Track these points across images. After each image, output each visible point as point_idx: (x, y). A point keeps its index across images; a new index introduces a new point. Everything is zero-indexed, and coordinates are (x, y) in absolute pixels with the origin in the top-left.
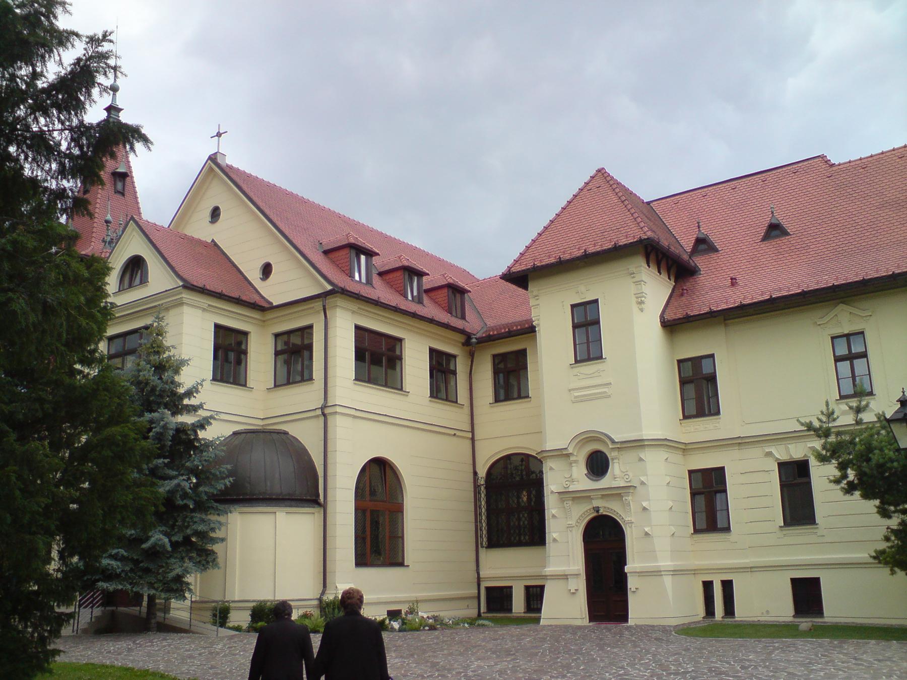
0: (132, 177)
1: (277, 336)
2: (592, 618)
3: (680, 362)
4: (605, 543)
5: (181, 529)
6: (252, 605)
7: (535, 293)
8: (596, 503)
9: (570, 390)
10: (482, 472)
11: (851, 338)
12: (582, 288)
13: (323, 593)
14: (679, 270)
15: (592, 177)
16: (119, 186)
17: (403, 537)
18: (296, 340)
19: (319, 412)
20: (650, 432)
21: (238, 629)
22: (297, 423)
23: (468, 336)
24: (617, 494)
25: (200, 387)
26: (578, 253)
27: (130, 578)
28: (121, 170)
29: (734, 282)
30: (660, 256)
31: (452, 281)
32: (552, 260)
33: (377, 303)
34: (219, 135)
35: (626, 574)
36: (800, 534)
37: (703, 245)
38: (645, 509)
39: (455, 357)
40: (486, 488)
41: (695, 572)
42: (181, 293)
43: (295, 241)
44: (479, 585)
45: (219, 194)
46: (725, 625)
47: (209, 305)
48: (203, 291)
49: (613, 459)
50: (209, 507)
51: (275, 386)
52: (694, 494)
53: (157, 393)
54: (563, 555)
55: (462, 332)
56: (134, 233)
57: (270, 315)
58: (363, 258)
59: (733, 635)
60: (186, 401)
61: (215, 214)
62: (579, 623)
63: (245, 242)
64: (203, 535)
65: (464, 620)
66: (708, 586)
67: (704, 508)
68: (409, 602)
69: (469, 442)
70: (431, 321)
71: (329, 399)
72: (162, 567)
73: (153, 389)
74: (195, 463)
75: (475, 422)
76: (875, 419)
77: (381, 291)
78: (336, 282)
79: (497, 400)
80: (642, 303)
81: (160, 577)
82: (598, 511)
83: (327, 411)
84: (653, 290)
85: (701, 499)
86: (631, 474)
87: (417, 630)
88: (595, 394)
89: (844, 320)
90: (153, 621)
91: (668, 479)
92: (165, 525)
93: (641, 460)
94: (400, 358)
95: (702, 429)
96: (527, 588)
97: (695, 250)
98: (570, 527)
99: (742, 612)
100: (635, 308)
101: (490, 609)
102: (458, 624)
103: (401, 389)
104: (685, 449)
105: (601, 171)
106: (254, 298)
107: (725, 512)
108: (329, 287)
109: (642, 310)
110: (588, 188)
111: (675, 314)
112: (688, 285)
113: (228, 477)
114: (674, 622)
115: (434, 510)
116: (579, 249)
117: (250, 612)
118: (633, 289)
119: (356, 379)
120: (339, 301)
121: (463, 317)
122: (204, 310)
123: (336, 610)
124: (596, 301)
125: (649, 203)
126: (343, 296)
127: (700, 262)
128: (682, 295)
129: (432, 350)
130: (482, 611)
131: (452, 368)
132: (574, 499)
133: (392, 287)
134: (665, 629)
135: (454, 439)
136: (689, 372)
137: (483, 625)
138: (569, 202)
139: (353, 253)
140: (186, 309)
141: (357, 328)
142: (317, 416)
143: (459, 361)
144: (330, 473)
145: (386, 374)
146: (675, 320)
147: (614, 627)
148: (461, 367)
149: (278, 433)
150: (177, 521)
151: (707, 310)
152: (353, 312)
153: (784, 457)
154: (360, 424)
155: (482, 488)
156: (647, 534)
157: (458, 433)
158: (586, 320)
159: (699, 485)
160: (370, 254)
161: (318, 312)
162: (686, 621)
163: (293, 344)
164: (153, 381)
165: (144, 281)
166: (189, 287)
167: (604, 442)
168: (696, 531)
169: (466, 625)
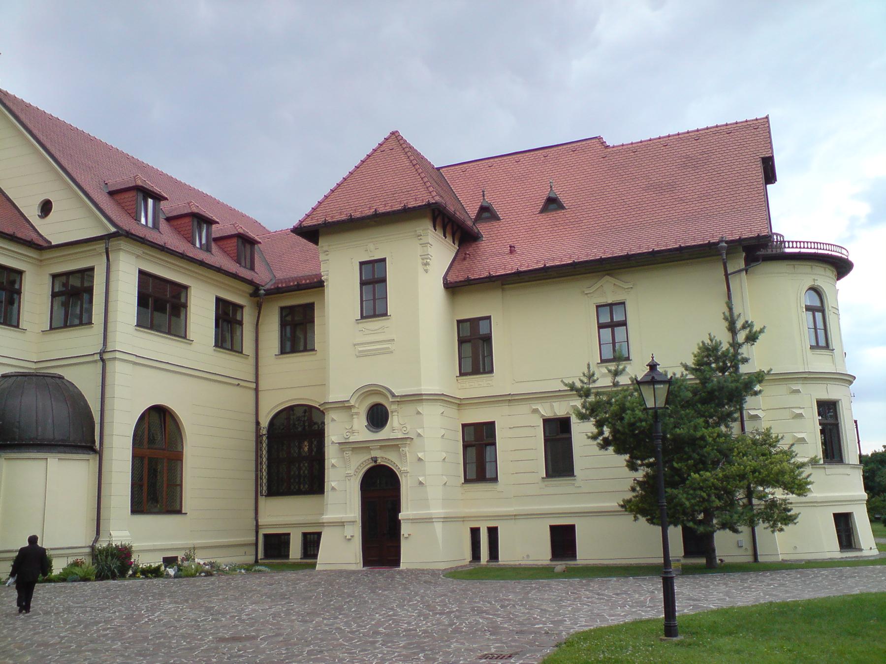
1: (54, 276)
2: (367, 562)
3: (459, 322)
4: (381, 491)
7: (325, 249)
8: (374, 454)
9: (355, 345)
10: (265, 423)
11: (614, 307)
12: (371, 246)
13: (96, 540)
14: (463, 235)
17: (181, 485)
18: (75, 282)
19: (97, 357)
20: (428, 388)
24: (395, 445)
26: (369, 212)
33: (162, 249)
36: (480, 490)
37: (486, 212)
38: (420, 459)
39: (241, 307)
40: (268, 438)
41: (464, 519)
43: (78, 180)
44: (257, 532)
49: (392, 412)
52: (465, 447)
54: (341, 503)
55: (250, 282)
57: (47, 255)
58: (150, 201)
62: (353, 568)
65: (240, 567)
66: (475, 532)
67: (474, 460)
69: (252, 394)
70: (219, 270)
71: (109, 344)
77: (168, 237)
79: (283, 351)
80: (427, 264)
82: (376, 462)
83: (106, 356)
84: (440, 252)
85: (472, 451)
86: (409, 428)
89: (609, 290)
91: (443, 432)
93: (419, 413)
94: (185, 306)
95: (477, 386)
96: (305, 535)
97: (479, 218)
98: (348, 476)
99: (505, 556)
100: (420, 268)
101: (267, 556)
103: (185, 337)
104: (460, 404)
107: (494, 464)
108: (113, 230)
109: (426, 271)
110: (382, 149)
111: (458, 277)
112: (470, 250)
114: (442, 566)
119: (138, 325)
120: (123, 244)
121: (252, 268)
124: (384, 260)
125: (438, 169)
127: (483, 229)
128: (464, 259)
129: (218, 300)
131: (239, 318)
132: (354, 449)
133: (179, 232)
134: (434, 573)
135: (238, 388)
137: (259, 571)
138: (363, 162)
139: (140, 197)
142: (95, 361)
147: (386, 571)
148: (248, 317)
149: (52, 377)
151: (486, 274)
152: (138, 257)
153: (549, 414)
155: (264, 438)
156: (421, 483)
157: (242, 383)
158: (373, 278)
159: (471, 438)
160: (158, 198)
161: (101, 254)
163: (72, 286)
168: (467, 481)
169: (243, 571)
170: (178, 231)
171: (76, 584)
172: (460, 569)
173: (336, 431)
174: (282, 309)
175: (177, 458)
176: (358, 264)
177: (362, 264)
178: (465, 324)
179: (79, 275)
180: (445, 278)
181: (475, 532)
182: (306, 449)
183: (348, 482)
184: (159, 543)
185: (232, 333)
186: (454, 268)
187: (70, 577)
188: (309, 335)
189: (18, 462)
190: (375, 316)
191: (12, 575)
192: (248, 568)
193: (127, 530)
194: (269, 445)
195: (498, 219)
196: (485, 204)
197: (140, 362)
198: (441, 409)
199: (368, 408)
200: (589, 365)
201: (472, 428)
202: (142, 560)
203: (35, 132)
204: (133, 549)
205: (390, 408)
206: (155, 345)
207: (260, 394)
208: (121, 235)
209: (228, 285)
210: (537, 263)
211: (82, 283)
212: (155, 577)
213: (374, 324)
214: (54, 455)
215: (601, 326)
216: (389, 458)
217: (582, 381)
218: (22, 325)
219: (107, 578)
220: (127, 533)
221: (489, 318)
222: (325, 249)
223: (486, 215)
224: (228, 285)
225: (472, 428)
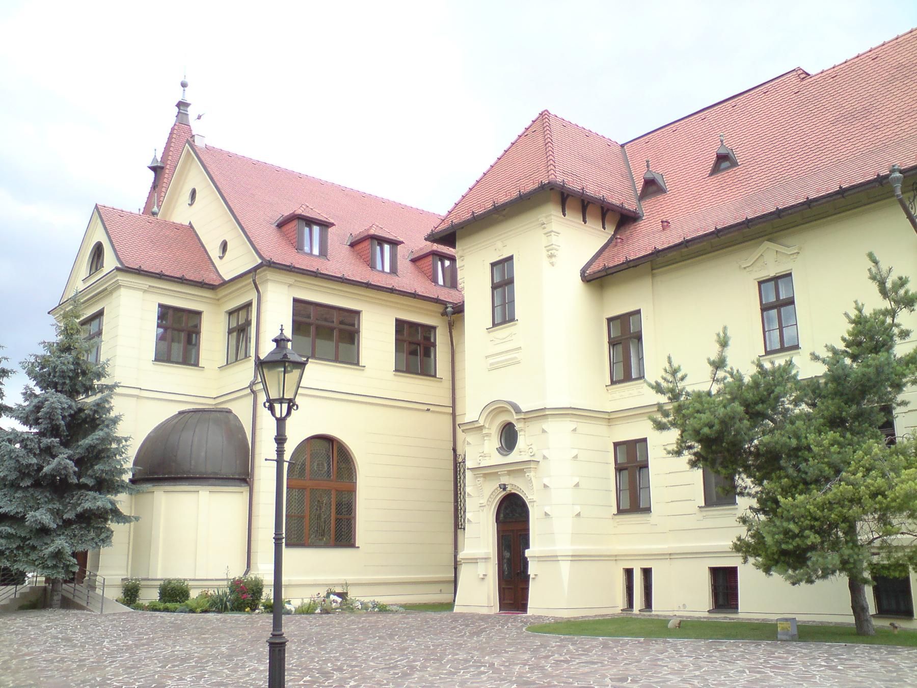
1: (231, 313)
2: (502, 607)
5: (75, 506)
6: (162, 582)
8: (504, 480)
9: (487, 357)
10: (290, 448)
11: (780, 282)
12: (499, 244)
13: (246, 573)
19: (249, 391)
22: (328, 401)
24: (519, 469)
27: (15, 556)
29: (665, 224)
39: (434, 328)
41: (616, 558)
42: (116, 276)
48: (139, 272)
55: (437, 301)
57: (222, 292)
61: (194, 192)
62: (485, 611)
66: (629, 573)
68: (327, 585)
76: (103, 359)
80: (551, 256)
82: (504, 489)
84: (577, 243)
88: (501, 362)
89: (770, 260)
93: (544, 431)
94: (358, 332)
99: (659, 606)
103: (358, 364)
104: (610, 418)
109: (552, 264)
118: (544, 241)
120: (270, 275)
122: (145, 291)
125: (622, 146)
132: (485, 475)
135: (428, 414)
140: (123, 291)
145: (337, 347)
152: (290, 285)
157: (432, 408)
158: (503, 280)
166: (125, 270)
167: (508, 411)
171: (157, 613)
180: (583, 272)
181: (629, 573)
189: (176, 494)
190: (504, 322)
198: (573, 425)
200: (669, 358)
205: (518, 426)
213: (505, 331)
214: (204, 487)
215: (765, 308)
216: (517, 485)
217: (665, 379)
224: (403, 305)
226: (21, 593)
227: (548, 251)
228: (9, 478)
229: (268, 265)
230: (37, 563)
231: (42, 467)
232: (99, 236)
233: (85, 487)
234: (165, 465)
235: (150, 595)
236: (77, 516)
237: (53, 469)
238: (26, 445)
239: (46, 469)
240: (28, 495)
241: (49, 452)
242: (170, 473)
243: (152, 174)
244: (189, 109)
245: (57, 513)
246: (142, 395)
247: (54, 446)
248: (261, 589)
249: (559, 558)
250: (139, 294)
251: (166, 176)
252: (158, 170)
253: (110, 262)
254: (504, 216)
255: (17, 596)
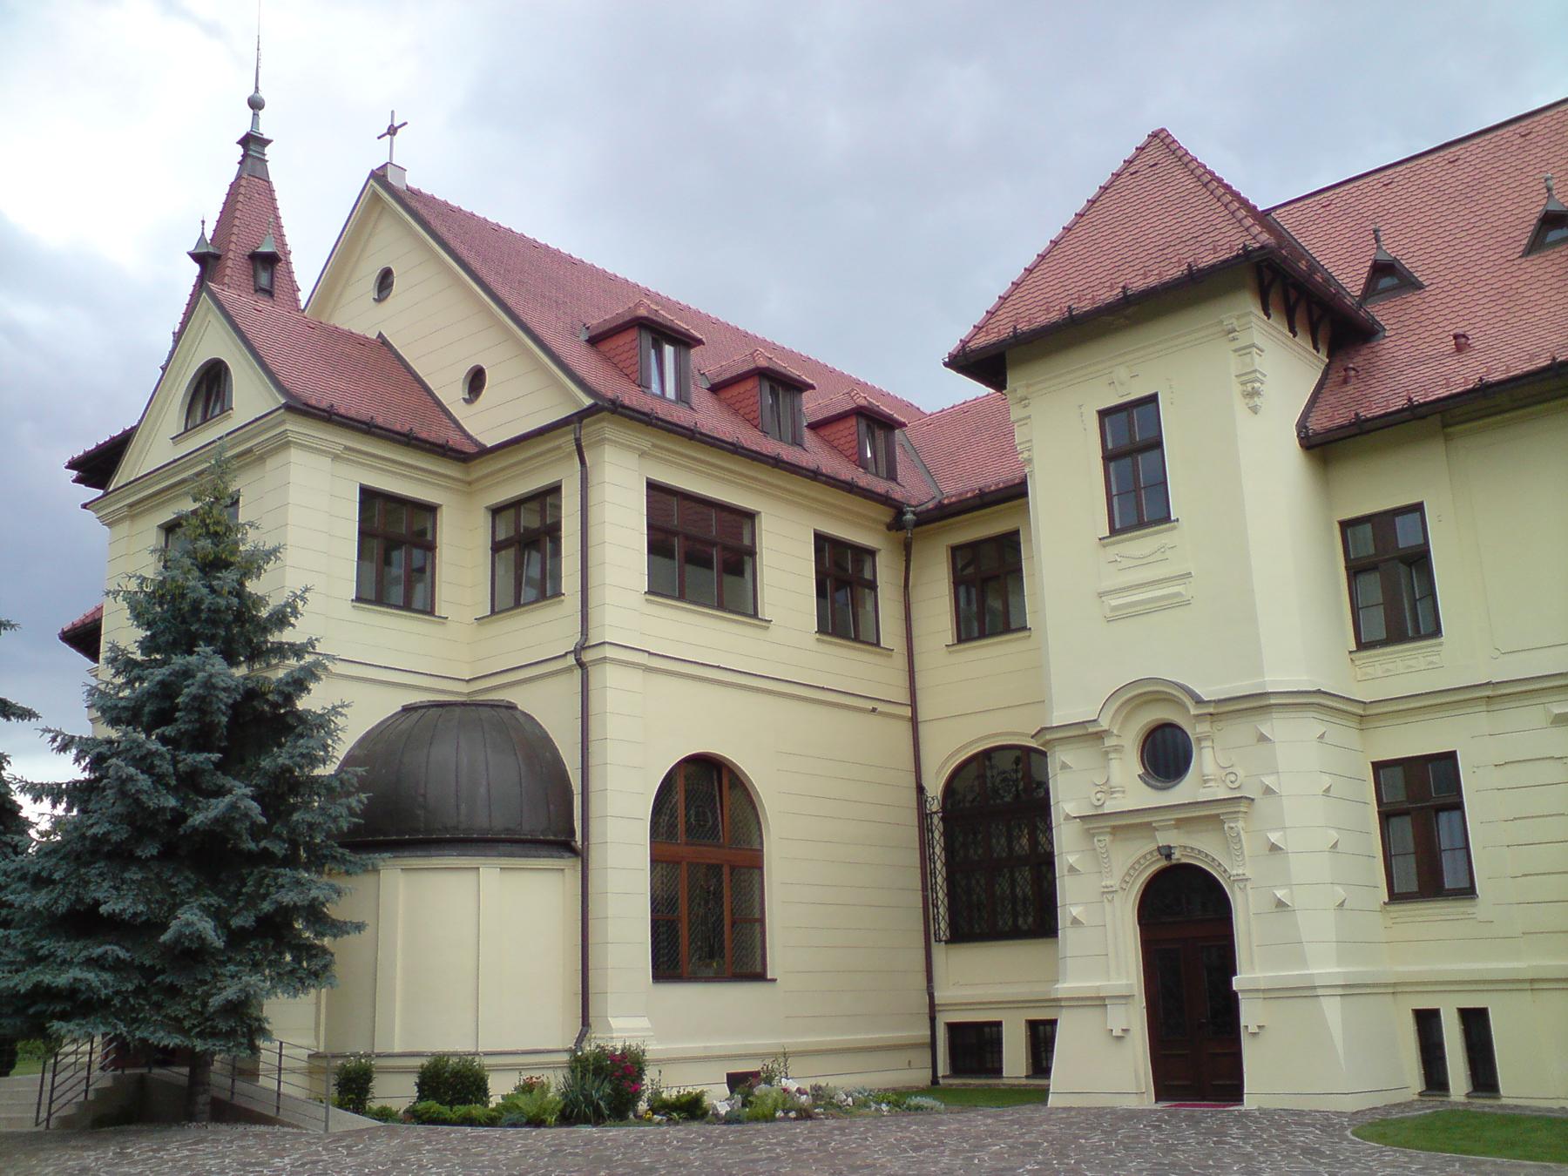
0: (289, 263)
1: (496, 511)
2: (1162, 1093)
3: (1345, 525)
4: (1187, 925)
5: (252, 901)
6: (425, 1061)
7: (1021, 392)
8: (1163, 839)
9: (1101, 595)
10: (935, 787)
12: (1122, 373)
14: (1334, 326)
15: (1140, 149)
16: (264, 279)
17: (762, 921)
18: (530, 520)
19: (571, 660)
20: (1281, 676)
21: (384, 1115)
23: (898, 508)
24: (1211, 816)
25: (300, 604)
26: (1107, 295)
27: (133, 1009)
28: (266, 248)
29: (1461, 343)
30: (1293, 295)
31: (863, 402)
32: (1054, 316)
33: (691, 435)
34: (392, 131)
35: (1235, 994)
36: (1431, 920)
37: (1388, 275)
38: (1274, 848)
39: (872, 553)
40: (943, 819)
41: (1395, 989)
43: (525, 318)
44: (933, 1020)
45: (392, 245)
46: (1476, 1115)
47: (346, 448)
49: (1199, 740)
50: (325, 857)
51: (493, 612)
52: (1386, 816)
53: (204, 616)
54: (1098, 952)
55: (884, 500)
56: (210, 317)
57: (481, 469)
58: (669, 351)
59: (1506, 1147)
60: (275, 637)
61: (385, 281)
62: (1132, 1103)
63: (435, 330)
64: (315, 914)
65: (881, 1096)
66: (1427, 1022)
67: (1411, 847)
69: (904, 729)
70: (814, 475)
71: (591, 633)
72: (205, 982)
73: (196, 607)
74: (280, 761)
75: (919, 685)
77: (709, 416)
78: (602, 390)
79: (961, 639)
80: (1254, 393)
81: (196, 1005)
82: (1168, 857)
83: (588, 656)
85: (1404, 828)
86: (1241, 772)
87: (769, 1118)
90: (202, 1099)
91: (1326, 781)
92: (220, 894)
93: (1263, 738)
94: (752, 552)
95: (1403, 670)
97: (1370, 290)
98: (1108, 892)
100: (1240, 405)
101: (957, 1069)
102: (866, 1105)
103: (755, 615)
104: (1364, 715)
105: (1160, 137)
106: (455, 439)
107: (1461, 854)
108: (588, 401)
109: (1255, 410)
110: (1132, 170)
111: (1331, 419)
112: (1358, 361)
113: (358, 791)
114: (1350, 1105)
115: (833, 863)
116: (1112, 288)
117: (415, 1079)
118: (1234, 364)
119: (650, 592)
120: (609, 429)
121: (892, 476)
122: (336, 457)
123: (590, 1076)
124: (1153, 398)
125: (1268, 212)
126: (616, 417)
127: (1381, 312)
128: (1345, 381)
129: (821, 540)
130: (940, 1073)
131: (868, 575)
132: (1115, 830)
133: (736, 412)
134: (1328, 1123)
135: (873, 718)
136: (1366, 544)
137: (918, 1108)
138: (1092, 202)
139: (647, 340)
140: (294, 454)
141: (652, 486)
142: (569, 669)
143: (881, 560)
144: (594, 785)
146: (1329, 431)
147: (1209, 1114)
148: (886, 573)
149: (492, 706)
150: (245, 885)
151: (1401, 403)
152: (643, 454)
154: (651, 680)
155: (936, 820)
156: (1280, 904)
157: (881, 707)
158: (1133, 451)
159: (1398, 795)
160: (684, 342)
161: (569, 455)
162: (1379, 1101)
163: (526, 529)
164: (194, 589)
165: (226, 409)
166: (298, 408)
168: (1395, 897)
169: (884, 1107)
170: (734, 409)
172: (1395, 1115)
173: (1072, 791)
174: (955, 550)
175: (754, 863)
176: (1095, 417)
177: (1103, 414)
178: (1360, 528)
179: (534, 505)
180: (1302, 426)
182: (1024, 841)
183: (1108, 906)
184: (719, 1044)
185: (856, 604)
186: (1321, 403)
187: (506, 1117)
188: (1012, 599)
191: (503, 1097)
192: (899, 1099)
193: (652, 1020)
194: (946, 834)
195: (1418, 286)
196: (1381, 257)
197: (658, 665)
198: (1320, 728)
199: (1140, 738)
201: (1398, 771)
202: (669, 1083)
203: (453, 243)
204: (648, 1056)
205: (1194, 731)
206: (692, 631)
207: (922, 729)
208: (602, 409)
209: (832, 505)
210: (1530, 360)
211: (543, 518)
212: (686, 1119)
218: (440, 609)
219: (586, 1121)
220: (644, 1023)
221: (1418, 508)
222: (1021, 392)
223: (1386, 282)
224: (832, 505)
225: (1398, 771)
226: (97, 1090)
227: (1243, 384)
228: (114, 838)
229: (608, 408)
230: (187, 1024)
231: (185, 817)
232: (215, 343)
233: (266, 857)
234: (400, 817)
235: (396, 1091)
236: (259, 920)
237: (216, 820)
238: (152, 766)
239: (198, 819)
240: (152, 876)
241: (191, 784)
242: (418, 831)
243: (195, 269)
244: (267, 150)
245: (218, 916)
246: (361, 669)
247: (204, 771)
248: (641, 1071)
249: (1320, 992)
250: (326, 462)
251: (228, 271)
252: (211, 261)
253: (249, 396)
254: (1127, 318)
255: (91, 1096)
